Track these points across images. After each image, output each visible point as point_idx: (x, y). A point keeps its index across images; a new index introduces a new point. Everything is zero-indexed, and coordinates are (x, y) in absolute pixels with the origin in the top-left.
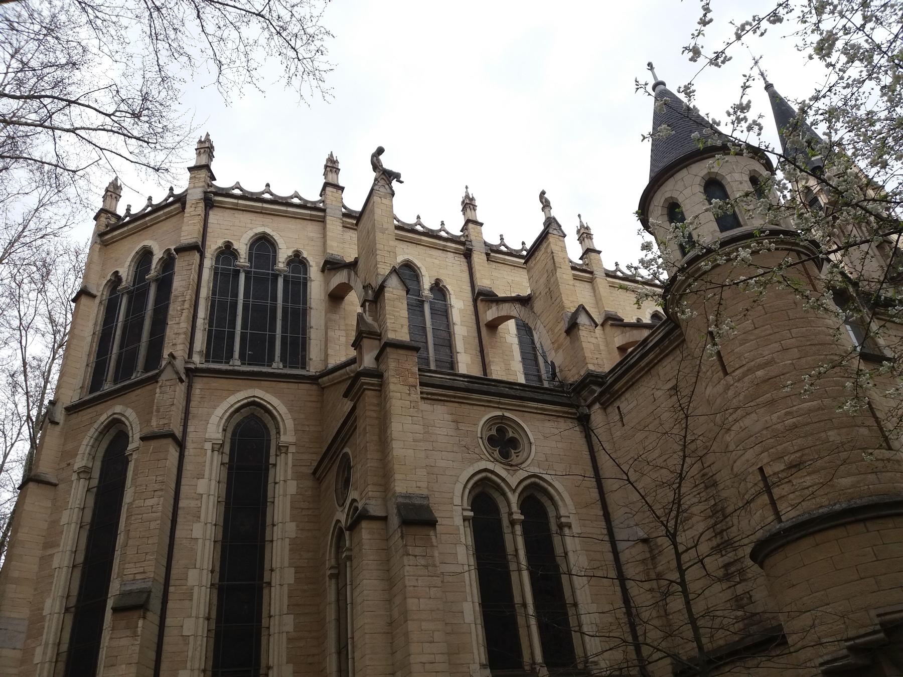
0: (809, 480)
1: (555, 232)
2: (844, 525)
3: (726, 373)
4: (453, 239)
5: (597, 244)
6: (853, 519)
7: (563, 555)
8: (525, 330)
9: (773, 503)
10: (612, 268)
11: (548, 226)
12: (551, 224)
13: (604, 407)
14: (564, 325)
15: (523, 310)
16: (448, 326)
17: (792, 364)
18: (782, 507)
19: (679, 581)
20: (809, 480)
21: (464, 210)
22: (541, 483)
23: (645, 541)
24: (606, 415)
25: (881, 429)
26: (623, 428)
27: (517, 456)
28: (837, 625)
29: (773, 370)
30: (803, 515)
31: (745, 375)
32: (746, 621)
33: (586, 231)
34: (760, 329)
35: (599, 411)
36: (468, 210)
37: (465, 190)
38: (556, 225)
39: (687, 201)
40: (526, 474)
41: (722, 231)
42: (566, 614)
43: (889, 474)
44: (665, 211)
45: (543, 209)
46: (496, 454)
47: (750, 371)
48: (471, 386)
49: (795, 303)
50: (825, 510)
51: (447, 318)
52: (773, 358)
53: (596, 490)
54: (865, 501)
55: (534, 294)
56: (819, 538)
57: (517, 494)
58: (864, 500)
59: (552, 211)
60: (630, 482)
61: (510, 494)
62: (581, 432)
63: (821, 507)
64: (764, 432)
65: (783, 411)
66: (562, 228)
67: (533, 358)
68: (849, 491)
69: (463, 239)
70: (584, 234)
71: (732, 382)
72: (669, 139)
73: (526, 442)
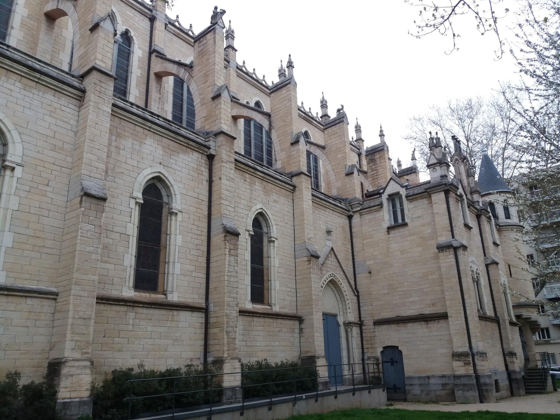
5: (236, 44)
8: (179, 83)
10: (241, 64)
14: (290, 140)
69: (151, 8)
70: (358, 129)
72: (496, 176)
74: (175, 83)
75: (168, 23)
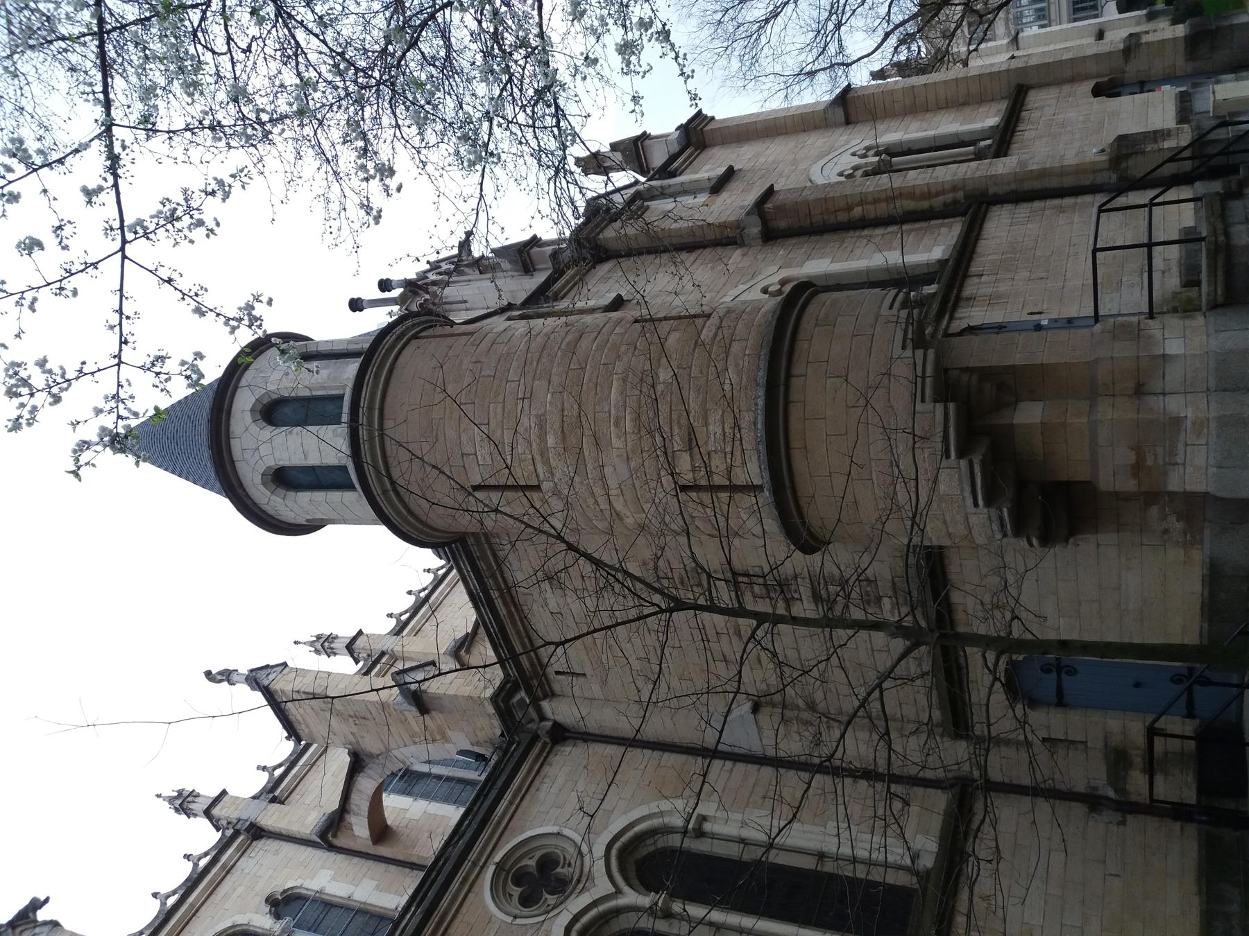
0: (715, 428)
1: (271, 677)
2: (787, 403)
3: (537, 488)
4: (222, 847)
6: (782, 388)
7: (742, 845)
8: (409, 781)
9: (733, 488)
11: (257, 683)
12: (256, 679)
13: (551, 695)
14: (412, 712)
15: (370, 771)
16: (347, 909)
17: (553, 393)
18: (740, 478)
19: (754, 623)
20: (715, 428)
21: (189, 813)
22: (624, 839)
23: (756, 709)
24: (564, 696)
25: (680, 318)
26: (588, 676)
27: (569, 865)
28: (924, 461)
29: (553, 422)
30: (759, 452)
31: (547, 462)
32: (901, 600)
33: (322, 640)
34: (491, 420)
35: (553, 704)
36: (192, 806)
37: (161, 799)
38: (264, 672)
39: (277, 454)
40: (601, 863)
41: (339, 423)
42: (832, 877)
43: (740, 326)
44: (281, 491)
45: (231, 683)
46: (551, 899)
47: (543, 453)
48: (426, 904)
49: (475, 362)
50: (760, 419)
51: (336, 906)
52: (536, 416)
53: (666, 755)
54: (763, 364)
55: (350, 743)
56: (795, 443)
57: (626, 889)
58: (762, 366)
59: (240, 671)
60: (562, 643)
61: (622, 901)
62: (575, 745)
63: (755, 424)
64: (633, 464)
65: (612, 428)
66: (271, 664)
67: (463, 786)
68: (744, 379)
69: (229, 832)
70: (324, 645)
71: (552, 484)
73: (553, 841)
74: (405, 792)
75: (271, 795)
